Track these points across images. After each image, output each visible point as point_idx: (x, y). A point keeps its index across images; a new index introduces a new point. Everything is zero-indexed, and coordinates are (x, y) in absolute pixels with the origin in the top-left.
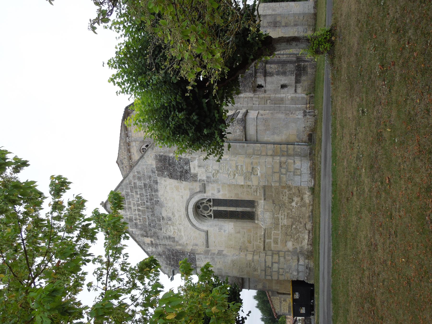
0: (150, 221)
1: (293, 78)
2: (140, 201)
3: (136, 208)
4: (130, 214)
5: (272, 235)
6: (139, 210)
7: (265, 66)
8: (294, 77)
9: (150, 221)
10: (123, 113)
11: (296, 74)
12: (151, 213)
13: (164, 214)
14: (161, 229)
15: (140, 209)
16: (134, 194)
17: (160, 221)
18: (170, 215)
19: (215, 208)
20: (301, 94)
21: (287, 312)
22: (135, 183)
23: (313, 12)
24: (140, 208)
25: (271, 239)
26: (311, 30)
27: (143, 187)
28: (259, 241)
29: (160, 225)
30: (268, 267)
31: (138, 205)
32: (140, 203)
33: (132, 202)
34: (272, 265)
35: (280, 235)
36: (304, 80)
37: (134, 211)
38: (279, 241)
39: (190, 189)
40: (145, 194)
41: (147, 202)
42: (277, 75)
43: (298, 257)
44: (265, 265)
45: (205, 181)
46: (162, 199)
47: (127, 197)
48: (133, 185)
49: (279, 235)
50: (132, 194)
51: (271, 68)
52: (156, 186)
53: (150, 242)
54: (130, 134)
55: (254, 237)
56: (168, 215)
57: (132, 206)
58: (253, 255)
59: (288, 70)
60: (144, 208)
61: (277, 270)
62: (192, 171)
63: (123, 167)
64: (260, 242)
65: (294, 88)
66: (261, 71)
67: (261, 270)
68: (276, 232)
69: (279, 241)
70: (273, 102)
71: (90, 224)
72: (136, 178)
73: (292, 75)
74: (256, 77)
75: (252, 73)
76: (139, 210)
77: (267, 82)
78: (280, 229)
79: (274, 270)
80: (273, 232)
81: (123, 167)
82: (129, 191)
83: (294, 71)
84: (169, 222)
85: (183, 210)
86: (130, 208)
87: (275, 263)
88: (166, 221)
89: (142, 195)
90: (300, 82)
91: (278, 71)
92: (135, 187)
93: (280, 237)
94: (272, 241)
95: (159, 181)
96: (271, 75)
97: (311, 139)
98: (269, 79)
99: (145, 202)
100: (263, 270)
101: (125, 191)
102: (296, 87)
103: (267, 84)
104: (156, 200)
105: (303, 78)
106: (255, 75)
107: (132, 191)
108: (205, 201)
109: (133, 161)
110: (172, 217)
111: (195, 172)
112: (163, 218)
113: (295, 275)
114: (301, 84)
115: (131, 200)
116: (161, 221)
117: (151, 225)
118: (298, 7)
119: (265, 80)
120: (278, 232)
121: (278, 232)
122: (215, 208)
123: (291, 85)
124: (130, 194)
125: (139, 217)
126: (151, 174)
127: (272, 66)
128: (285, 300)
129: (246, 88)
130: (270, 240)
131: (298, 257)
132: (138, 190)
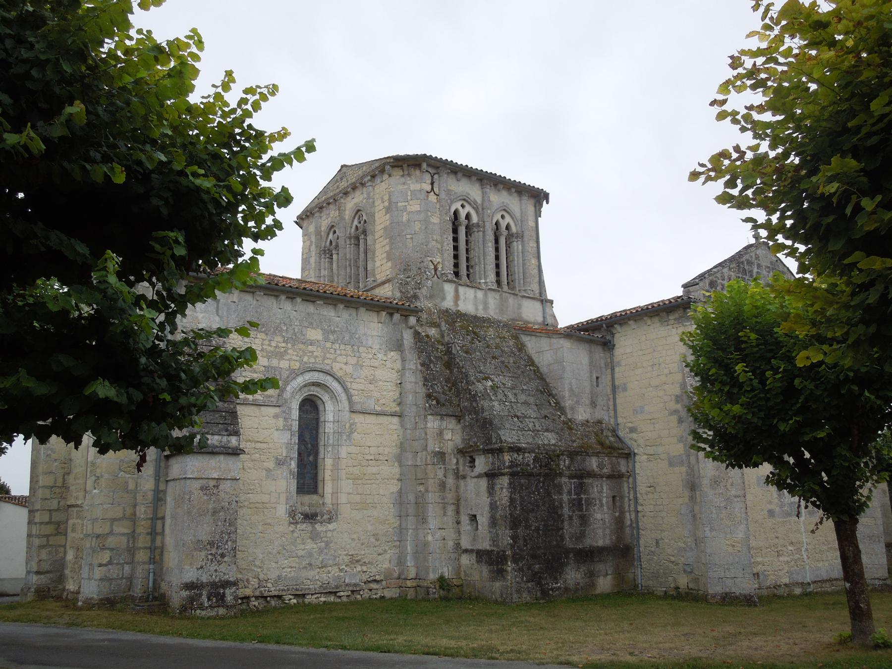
1: (485, 545)
7: (503, 474)
8: (488, 548)
10: (411, 153)
11: (492, 551)
20: (440, 567)
23: (710, 591)
26: (691, 586)
36: (481, 572)
42: (491, 504)
43: (48, 572)
51: (502, 488)
54: (378, 180)
58: (52, 487)
59: (500, 532)
63: (337, 181)
65: (470, 548)
66: (497, 464)
70: (420, 500)
71: (764, 64)
73: (491, 543)
74: (486, 452)
75: (491, 443)
77: (479, 479)
81: (337, 181)
83: (497, 546)
90: (478, 562)
91: (497, 507)
96: (491, 490)
97: (155, 602)
98: (484, 483)
102: (472, 551)
103: (476, 480)
105: (485, 570)
109: (342, 201)
114: (476, 565)
118: (730, 549)
119: (479, 476)
123: (474, 540)
127: (504, 490)
129: (468, 430)
131: (48, 572)
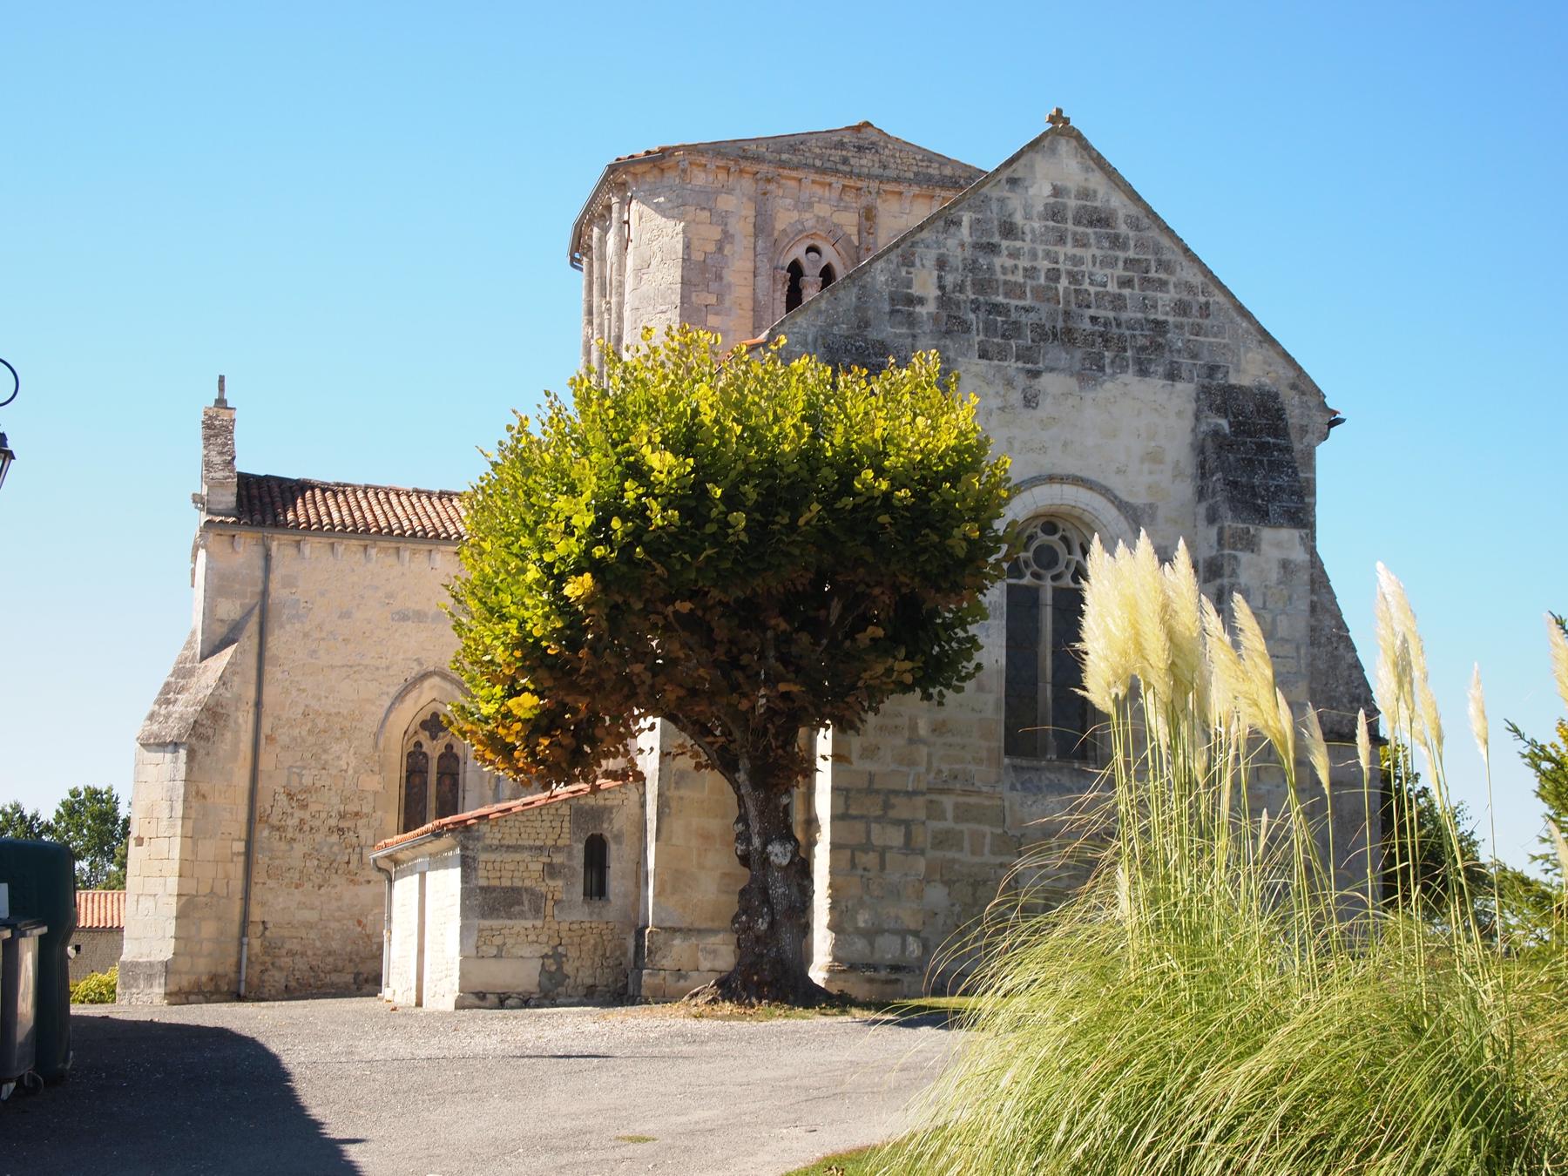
0: (1014, 316)
2: (1092, 290)
3: (1060, 266)
4: (1033, 231)
5: (975, 826)
6: (1054, 275)
9: (1014, 316)
12: (1048, 326)
13: (1050, 383)
14: (983, 355)
15: (1057, 279)
16: (1119, 271)
17: (1018, 359)
18: (1047, 408)
19: (1047, 596)
21: (483, 882)
22: (1163, 284)
24: (1064, 282)
25: (957, 819)
27: (1152, 317)
28: (945, 767)
29: (1003, 355)
30: (887, 806)
31: (1074, 278)
32: (1086, 285)
33: (1086, 254)
34: (898, 822)
35: (976, 859)
37: (1047, 254)
38: (950, 855)
39: (1151, 506)
40: (1124, 316)
41: (1094, 319)
44: (896, 793)
45: (1233, 580)
46: (1110, 388)
47: (1108, 236)
48: (1152, 274)
49: (973, 853)
50: (1121, 264)
52: (1161, 370)
53: (916, 291)
55: (963, 747)
56: (1049, 400)
57: (1069, 249)
60: (1068, 303)
61: (877, 840)
62: (1267, 535)
64: (940, 771)
67: (871, 776)
68: (988, 840)
69: (950, 855)
72: (1186, 297)
76: (1054, 275)
78: (999, 860)
79: (875, 827)
80: (987, 829)
82: (1131, 254)
84: (1016, 397)
85: (1070, 466)
86: (1061, 240)
87: (908, 836)
88: (1021, 380)
89: (1118, 302)
92: (1148, 280)
93: (965, 856)
94: (949, 824)
95: (1179, 386)
99: (1092, 312)
100: (871, 781)
101: (1131, 234)
104: (1107, 361)
106: (695, 755)
107: (1128, 263)
108: (1078, 556)
110: (1040, 413)
111: (1264, 547)
112: (1035, 374)
113: (855, 920)
115: (1094, 250)
116: (1020, 364)
117: (999, 314)
120: (987, 849)
121: (987, 849)
122: (1047, 596)
124: (1121, 255)
125: (1025, 270)
126: (1206, 358)
128: (551, 871)
130: (950, 814)
132: (1137, 291)
